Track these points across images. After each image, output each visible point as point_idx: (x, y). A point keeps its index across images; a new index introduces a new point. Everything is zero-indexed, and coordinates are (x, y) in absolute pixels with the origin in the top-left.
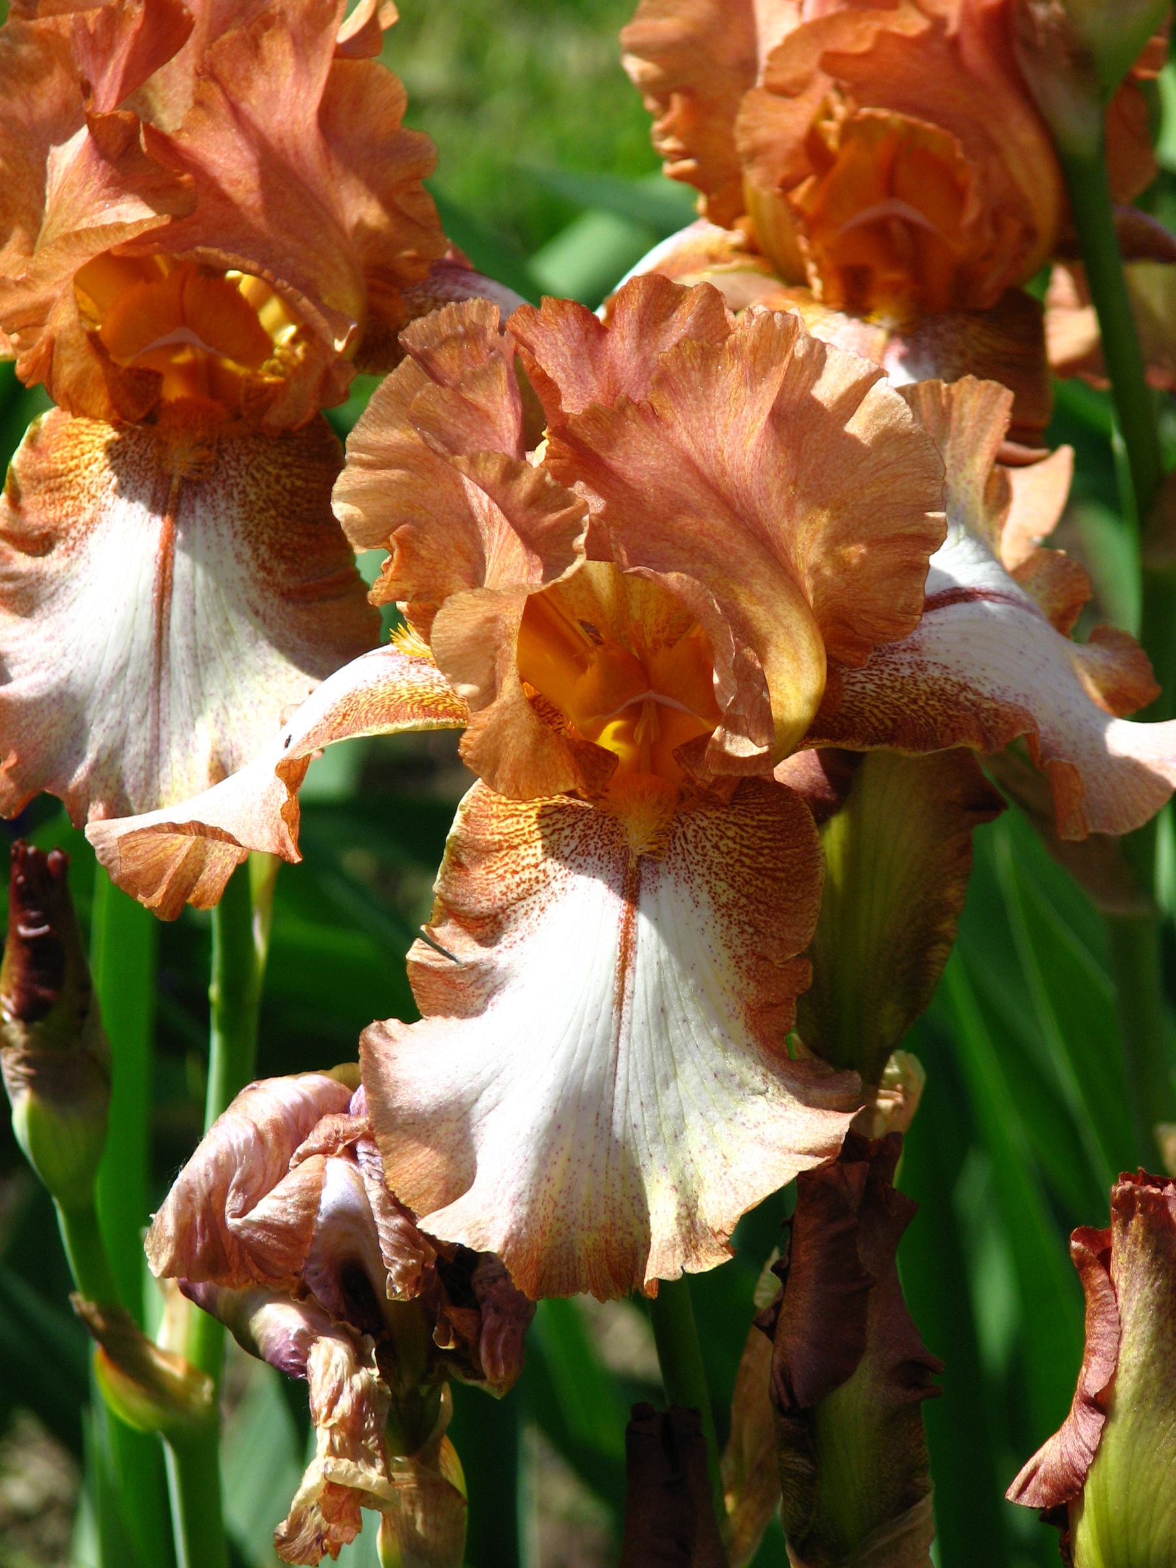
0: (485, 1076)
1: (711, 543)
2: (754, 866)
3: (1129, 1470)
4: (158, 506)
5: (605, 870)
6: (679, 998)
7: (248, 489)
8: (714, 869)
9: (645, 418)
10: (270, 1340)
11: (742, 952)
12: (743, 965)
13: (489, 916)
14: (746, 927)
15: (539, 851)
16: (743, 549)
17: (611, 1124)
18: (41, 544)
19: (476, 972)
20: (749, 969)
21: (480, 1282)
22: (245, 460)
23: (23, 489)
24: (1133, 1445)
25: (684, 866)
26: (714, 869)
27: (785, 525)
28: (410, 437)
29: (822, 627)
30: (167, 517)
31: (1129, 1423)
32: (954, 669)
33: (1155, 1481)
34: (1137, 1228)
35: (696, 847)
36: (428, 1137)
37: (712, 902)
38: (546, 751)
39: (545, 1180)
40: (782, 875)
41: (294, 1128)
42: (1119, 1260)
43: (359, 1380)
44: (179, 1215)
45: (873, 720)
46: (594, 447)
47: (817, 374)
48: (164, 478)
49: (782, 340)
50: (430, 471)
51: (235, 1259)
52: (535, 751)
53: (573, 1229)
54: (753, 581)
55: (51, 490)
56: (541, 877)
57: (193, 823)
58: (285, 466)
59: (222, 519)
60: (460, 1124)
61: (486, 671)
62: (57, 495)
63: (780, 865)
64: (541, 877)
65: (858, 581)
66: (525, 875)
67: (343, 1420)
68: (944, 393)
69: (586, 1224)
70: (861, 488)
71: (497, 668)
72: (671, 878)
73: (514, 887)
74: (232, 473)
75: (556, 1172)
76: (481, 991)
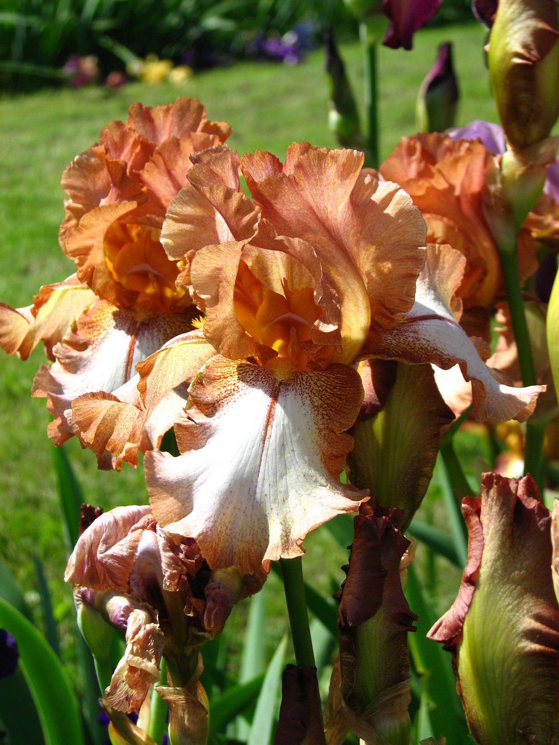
0: (201, 469)
1: (320, 247)
2: (332, 392)
3: (486, 613)
4: (129, 332)
5: (264, 387)
6: (291, 441)
7: (167, 329)
8: (314, 391)
9: (291, 183)
10: (114, 611)
11: (322, 427)
12: (322, 433)
13: (211, 404)
14: (325, 416)
15: (237, 378)
16: (334, 251)
17: (255, 494)
18: (83, 346)
19: (203, 427)
20: (325, 436)
21: (208, 589)
22: (167, 319)
23: (79, 328)
24: (488, 600)
25: (300, 388)
26: (314, 391)
27: (355, 249)
28: (195, 211)
29: (372, 305)
30: (133, 336)
31: (486, 589)
32: (433, 342)
33: (498, 619)
34: (494, 493)
35: (306, 383)
36: (172, 493)
37: (311, 404)
38: (244, 341)
39: (222, 515)
40: (344, 397)
41: (130, 522)
42: (485, 509)
43: (149, 627)
44: (78, 555)
45: (394, 351)
46: (269, 198)
47: (374, 191)
48: (134, 322)
49: (356, 162)
50: (204, 226)
51: (102, 577)
52: (239, 341)
53: (234, 540)
54: (338, 266)
55: (89, 328)
56: (236, 389)
57: (100, 392)
58: (183, 322)
59: (155, 338)
60: (188, 490)
61: (215, 290)
62: (91, 329)
63: (343, 393)
64: (236, 389)
65: (387, 279)
66: (229, 388)
67: (139, 640)
68: (437, 248)
69: (240, 539)
70: (390, 237)
71: (220, 290)
72: (293, 392)
73: (223, 392)
74: (161, 323)
75: (228, 512)
76: (204, 437)
